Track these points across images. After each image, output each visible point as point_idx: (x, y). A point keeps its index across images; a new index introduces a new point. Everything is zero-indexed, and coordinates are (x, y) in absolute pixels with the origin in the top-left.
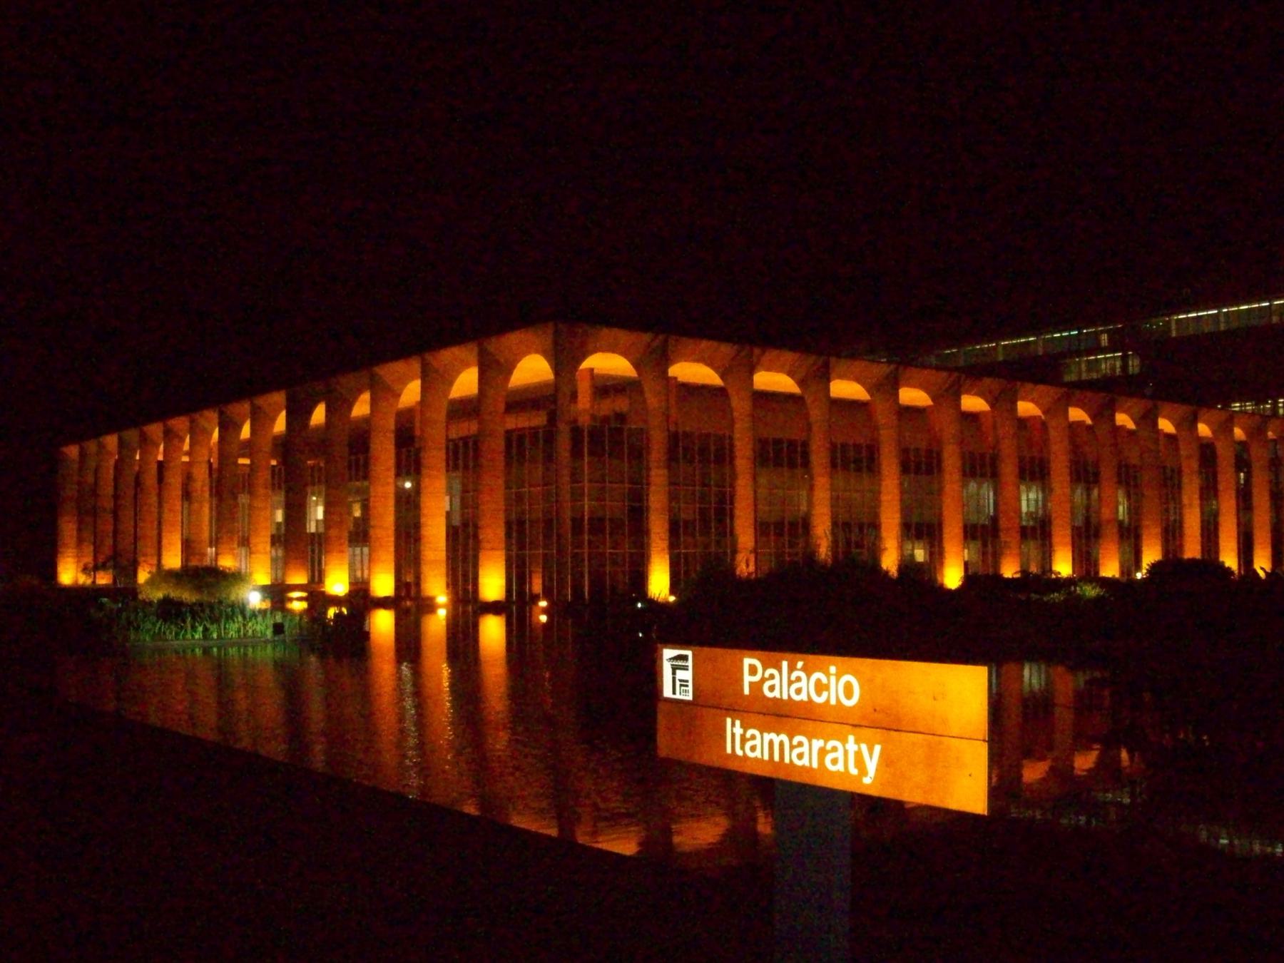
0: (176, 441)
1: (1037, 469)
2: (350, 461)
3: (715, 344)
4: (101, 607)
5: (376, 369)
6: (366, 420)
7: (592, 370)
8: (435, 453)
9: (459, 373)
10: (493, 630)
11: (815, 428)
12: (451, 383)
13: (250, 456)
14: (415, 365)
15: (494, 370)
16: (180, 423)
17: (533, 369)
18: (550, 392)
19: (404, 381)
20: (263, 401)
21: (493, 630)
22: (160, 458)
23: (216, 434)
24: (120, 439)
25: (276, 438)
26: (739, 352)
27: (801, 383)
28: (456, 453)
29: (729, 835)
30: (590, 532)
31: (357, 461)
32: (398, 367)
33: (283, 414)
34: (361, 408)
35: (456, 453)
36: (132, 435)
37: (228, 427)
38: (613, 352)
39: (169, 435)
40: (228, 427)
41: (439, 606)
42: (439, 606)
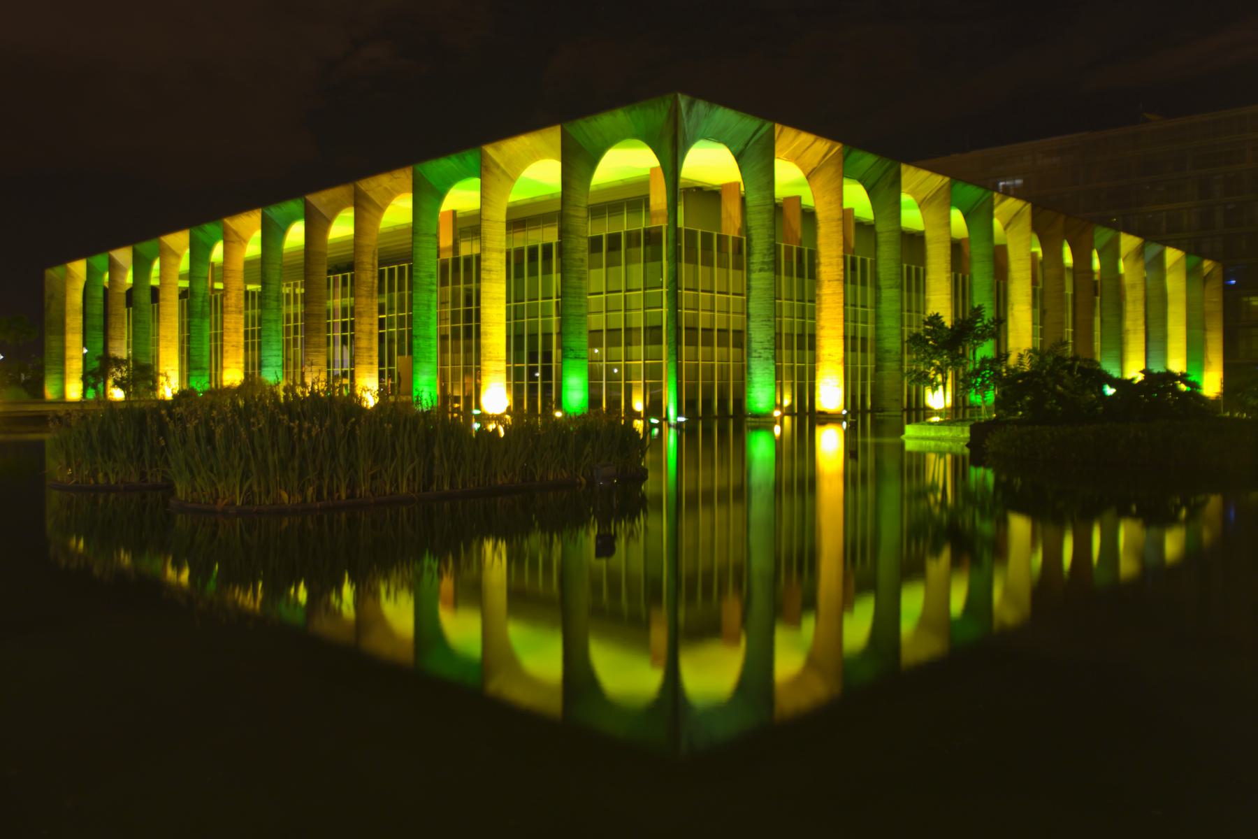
0: (173, 260)
1: (906, 314)
2: (381, 274)
4: (1175, 389)
5: (490, 150)
7: (454, 212)
8: (495, 255)
9: (524, 167)
10: (830, 445)
12: (381, 210)
13: (222, 280)
14: (404, 177)
15: (578, 160)
18: (349, 250)
19: (390, 195)
21: (830, 445)
22: (155, 282)
23: (107, 276)
25: (249, 263)
26: (830, 149)
28: (519, 264)
32: (384, 180)
33: (188, 251)
35: (519, 264)
36: (100, 260)
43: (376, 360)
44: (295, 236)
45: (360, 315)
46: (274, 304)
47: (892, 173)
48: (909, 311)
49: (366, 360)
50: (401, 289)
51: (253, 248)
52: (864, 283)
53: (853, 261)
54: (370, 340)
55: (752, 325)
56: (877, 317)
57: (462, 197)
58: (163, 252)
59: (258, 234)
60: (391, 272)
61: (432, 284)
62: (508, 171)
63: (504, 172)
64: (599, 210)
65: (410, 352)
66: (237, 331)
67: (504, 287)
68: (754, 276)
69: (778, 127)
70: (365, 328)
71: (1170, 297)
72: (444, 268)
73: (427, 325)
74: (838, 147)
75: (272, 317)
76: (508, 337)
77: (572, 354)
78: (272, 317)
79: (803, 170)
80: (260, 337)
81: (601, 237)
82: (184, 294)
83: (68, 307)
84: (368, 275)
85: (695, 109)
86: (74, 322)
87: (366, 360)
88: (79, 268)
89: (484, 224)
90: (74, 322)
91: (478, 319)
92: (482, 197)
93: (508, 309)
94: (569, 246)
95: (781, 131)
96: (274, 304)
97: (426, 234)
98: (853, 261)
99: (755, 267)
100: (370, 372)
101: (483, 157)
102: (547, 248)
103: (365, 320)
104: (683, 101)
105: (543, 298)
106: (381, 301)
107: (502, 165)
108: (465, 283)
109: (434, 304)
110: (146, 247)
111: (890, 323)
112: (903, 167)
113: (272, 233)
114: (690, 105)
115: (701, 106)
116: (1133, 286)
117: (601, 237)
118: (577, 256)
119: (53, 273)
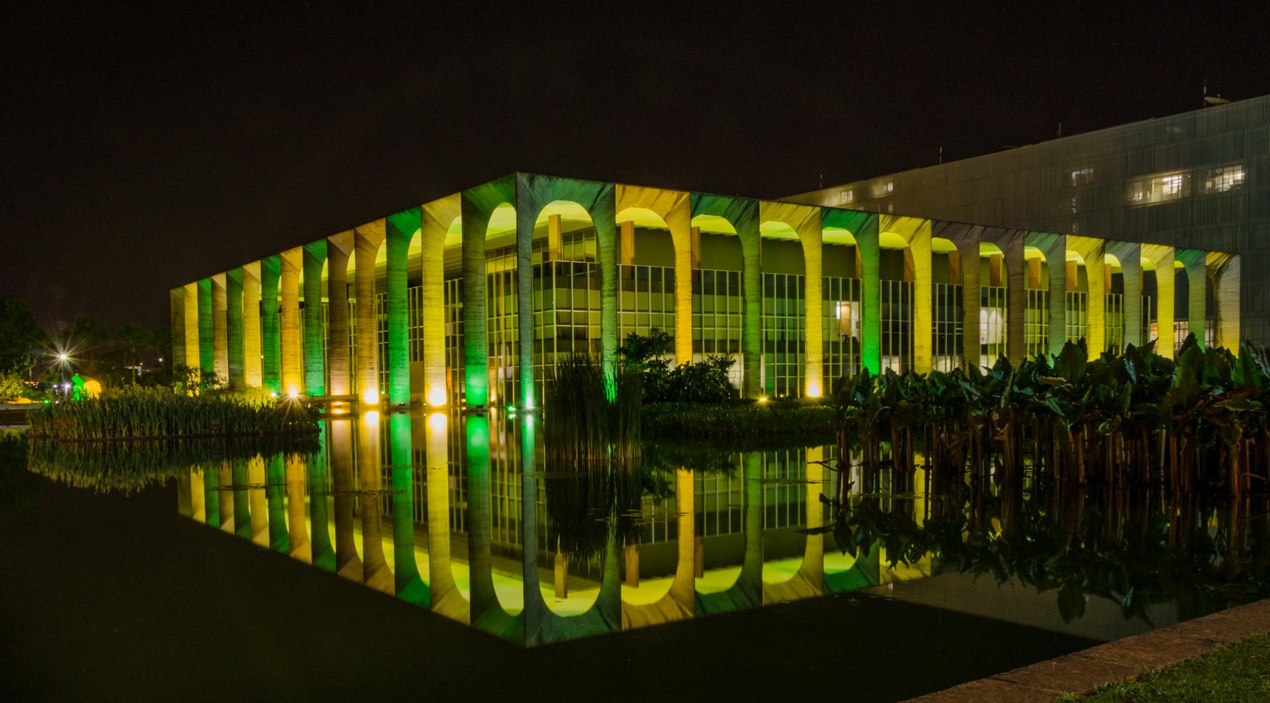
3: (656, 191)
5: (425, 207)
6: (421, 259)
8: (434, 287)
11: (747, 262)
16: (341, 239)
20: (364, 230)
24: (228, 277)
27: (735, 224)
29: (740, 583)
30: (559, 350)
31: (414, 291)
33: (353, 253)
34: (415, 245)
36: (206, 283)
37: (475, 216)
38: (570, 199)
39: (359, 243)
40: (475, 216)
41: (367, 408)
42: (367, 408)
43: (376, 366)
45: (361, 331)
46: (315, 322)
47: (752, 208)
49: (368, 366)
53: (769, 278)
54: (371, 350)
55: (604, 337)
56: (744, 326)
58: (359, 243)
59: (458, 221)
65: (422, 359)
66: (294, 343)
67: (443, 310)
68: (605, 300)
69: (619, 188)
70: (367, 341)
71: (1161, 290)
72: (536, 270)
73: (401, 339)
74: (686, 195)
75: (314, 332)
77: (473, 361)
78: (314, 332)
79: (660, 214)
80: (386, 339)
82: (302, 305)
83: (187, 322)
85: (536, 182)
86: (192, 335)
87: (368, 366)
88: (192, 288)
89: (425, 264)
90: (192, 335)
91: (422, 335)
92: (423, 243)
94: (469, 282)
95: (624, 189)
96: (315, 322)
98: (769, 278)
99: (605, 293)
100: (371, 375)
101: (423, 212)
102: (507, 274)
103: (366, 335)
104: (523, 179)
109: (406, 322)
110: (402, 219)
111: (753, 331)
112: (762, 204)
114: (531, 181)
115: (541, 180)
116: (1095, 284)
118: (478, 288)
119: (175, 293)
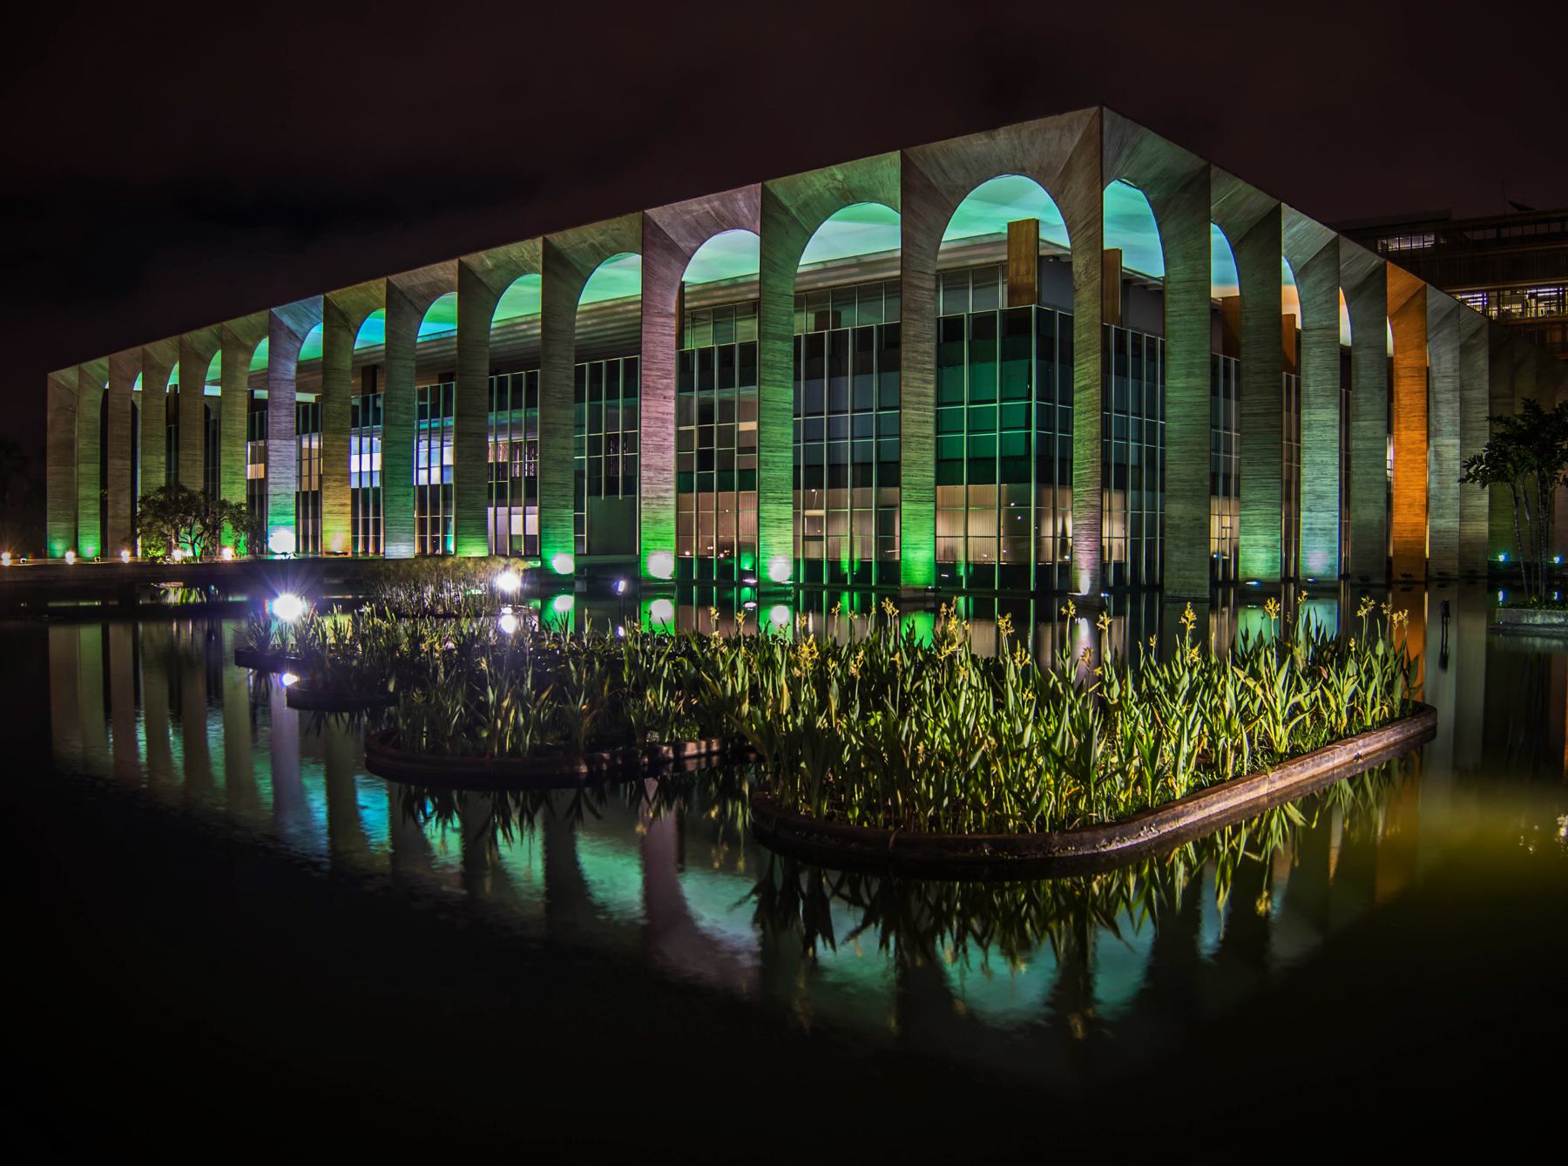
2: (580, 372)
8: (779, 345)
17: (726, 256)
32: (592, 233)
44: (372, 333)
48: (1289, 439)
50: (596, 396)
51: (313, 343)
52: (1227, 396)
57: (616, 281)
60: (502, 382)
61: (667, 387)
62: (802, 220)
63: (794, 220)
64: (953, 279)
76: (796, 468)
81: (961, 319)
84: (561, 375)
90: (87, 445)
93: (796, 425)
97: (660, 314)
105: (830, 413)
106: (705, 394)
107: (793, 211)
108: (608, 398)
113: (340, 325)
117: (961, 319)
